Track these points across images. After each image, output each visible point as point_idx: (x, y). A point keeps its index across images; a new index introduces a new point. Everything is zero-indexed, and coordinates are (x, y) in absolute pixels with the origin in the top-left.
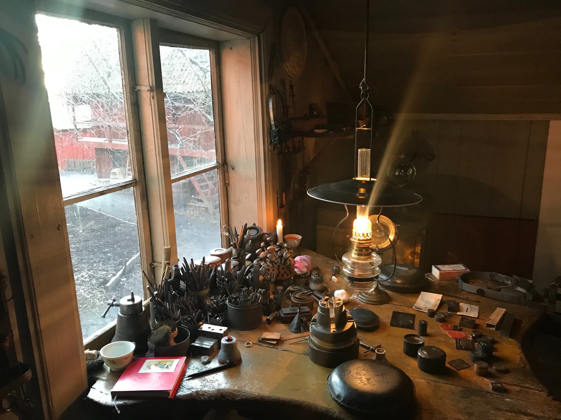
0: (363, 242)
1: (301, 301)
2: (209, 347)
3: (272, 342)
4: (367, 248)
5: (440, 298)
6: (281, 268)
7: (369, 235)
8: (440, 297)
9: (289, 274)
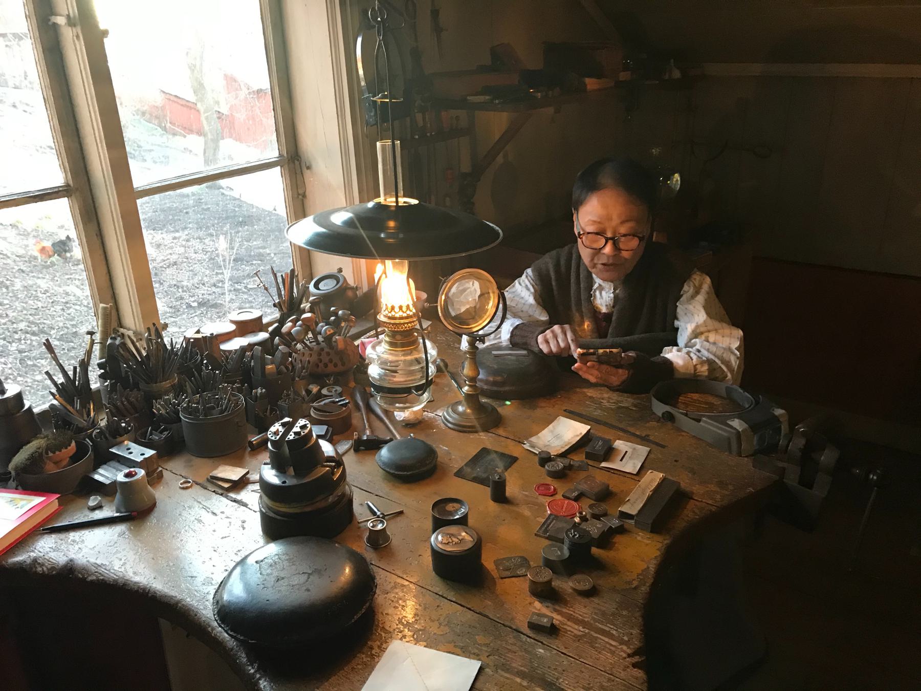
0: (402, 321)
1: (321, 416)
2: (107, 482)
3: (220, 483)
4: (408, 333)
5: (584, 432)
6: (323, 353)
7: (411, 307)
8: (582, 429)
9: (339, 364)
